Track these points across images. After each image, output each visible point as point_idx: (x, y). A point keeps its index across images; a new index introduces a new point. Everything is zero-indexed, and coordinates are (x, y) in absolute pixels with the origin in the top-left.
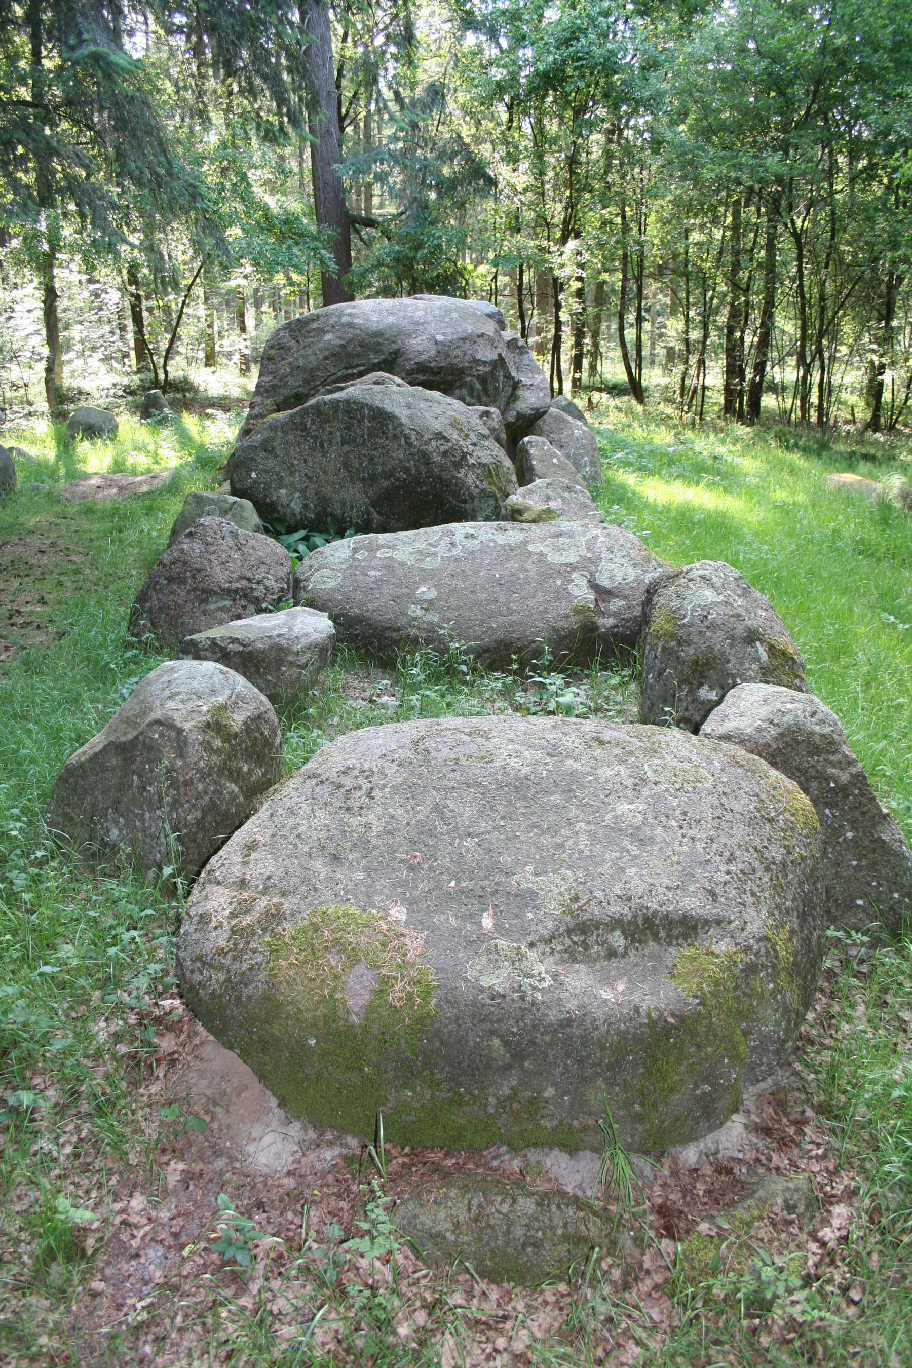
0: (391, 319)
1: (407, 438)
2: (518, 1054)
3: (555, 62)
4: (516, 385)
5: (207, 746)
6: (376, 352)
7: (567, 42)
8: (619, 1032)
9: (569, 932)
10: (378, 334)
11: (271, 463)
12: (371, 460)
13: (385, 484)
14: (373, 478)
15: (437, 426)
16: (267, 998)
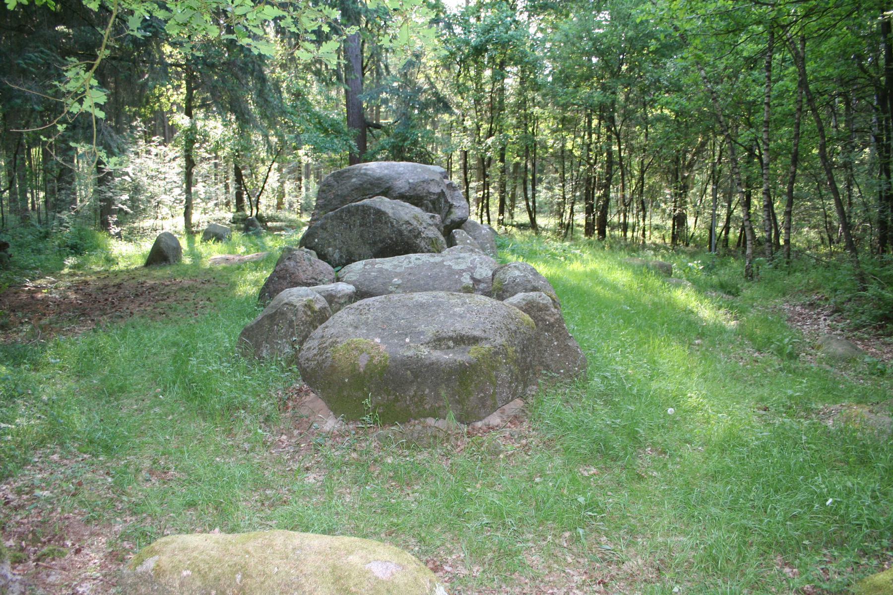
0: (386, 171)
1: (392, 223)
2: (416, 376)
3: (481, 41)
4: (451, 206)
5: (305, 313)
6: (378, 187)
7: (488, 31)
8: (450, 368)
9: (435, 341)
10: (379, 179)
11: (325, 235)
12: (374, 234)
13: (380, 245)
14: (375, 243)
15: (406, 218)
16: (332, 366)
